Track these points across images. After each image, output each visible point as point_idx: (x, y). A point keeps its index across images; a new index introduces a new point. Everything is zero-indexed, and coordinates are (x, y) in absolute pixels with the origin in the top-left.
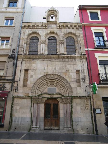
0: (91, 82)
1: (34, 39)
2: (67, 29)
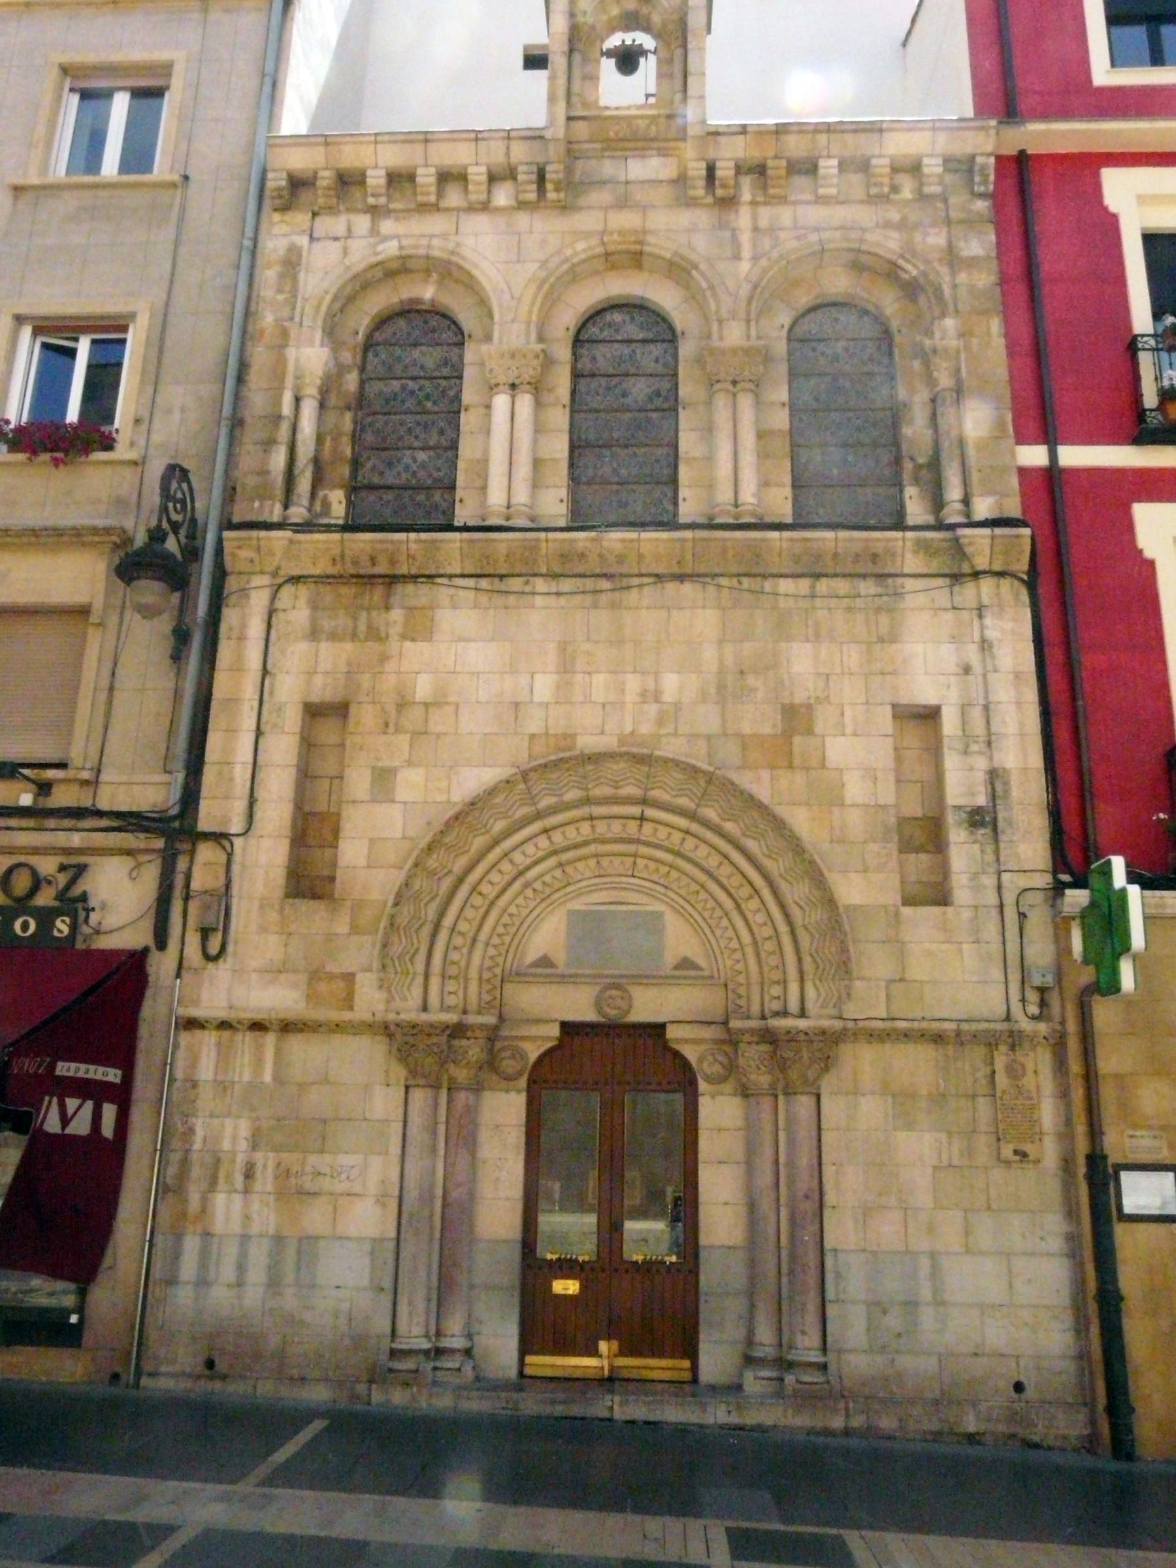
1: (410, 358)
2: (801, 210)
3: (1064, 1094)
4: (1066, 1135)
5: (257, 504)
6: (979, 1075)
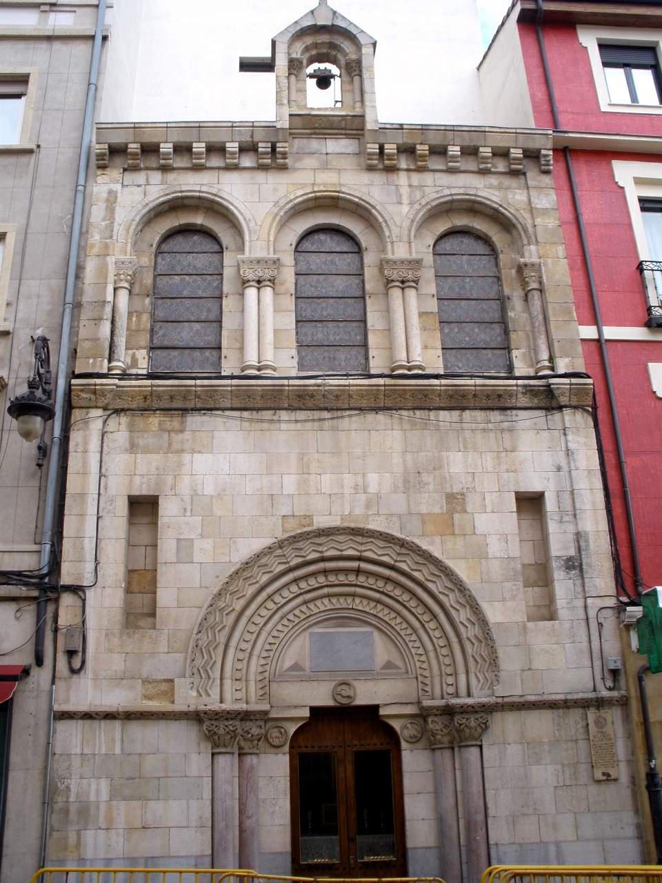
0: (630, 590)
3: (630, 736)
4: (631, 762)
5: (91, 361)
6: (579, 726)
